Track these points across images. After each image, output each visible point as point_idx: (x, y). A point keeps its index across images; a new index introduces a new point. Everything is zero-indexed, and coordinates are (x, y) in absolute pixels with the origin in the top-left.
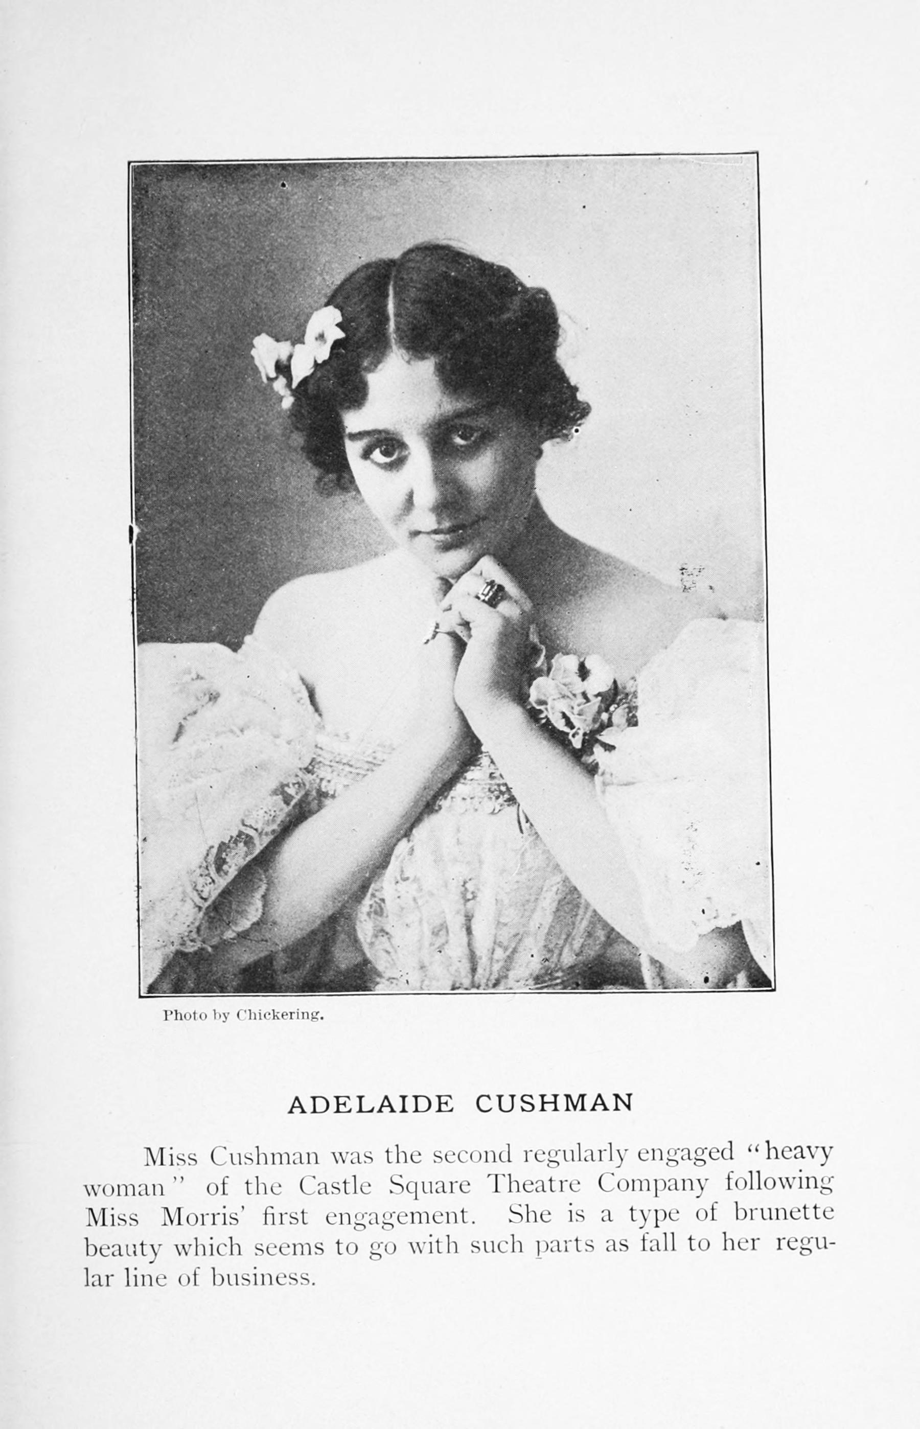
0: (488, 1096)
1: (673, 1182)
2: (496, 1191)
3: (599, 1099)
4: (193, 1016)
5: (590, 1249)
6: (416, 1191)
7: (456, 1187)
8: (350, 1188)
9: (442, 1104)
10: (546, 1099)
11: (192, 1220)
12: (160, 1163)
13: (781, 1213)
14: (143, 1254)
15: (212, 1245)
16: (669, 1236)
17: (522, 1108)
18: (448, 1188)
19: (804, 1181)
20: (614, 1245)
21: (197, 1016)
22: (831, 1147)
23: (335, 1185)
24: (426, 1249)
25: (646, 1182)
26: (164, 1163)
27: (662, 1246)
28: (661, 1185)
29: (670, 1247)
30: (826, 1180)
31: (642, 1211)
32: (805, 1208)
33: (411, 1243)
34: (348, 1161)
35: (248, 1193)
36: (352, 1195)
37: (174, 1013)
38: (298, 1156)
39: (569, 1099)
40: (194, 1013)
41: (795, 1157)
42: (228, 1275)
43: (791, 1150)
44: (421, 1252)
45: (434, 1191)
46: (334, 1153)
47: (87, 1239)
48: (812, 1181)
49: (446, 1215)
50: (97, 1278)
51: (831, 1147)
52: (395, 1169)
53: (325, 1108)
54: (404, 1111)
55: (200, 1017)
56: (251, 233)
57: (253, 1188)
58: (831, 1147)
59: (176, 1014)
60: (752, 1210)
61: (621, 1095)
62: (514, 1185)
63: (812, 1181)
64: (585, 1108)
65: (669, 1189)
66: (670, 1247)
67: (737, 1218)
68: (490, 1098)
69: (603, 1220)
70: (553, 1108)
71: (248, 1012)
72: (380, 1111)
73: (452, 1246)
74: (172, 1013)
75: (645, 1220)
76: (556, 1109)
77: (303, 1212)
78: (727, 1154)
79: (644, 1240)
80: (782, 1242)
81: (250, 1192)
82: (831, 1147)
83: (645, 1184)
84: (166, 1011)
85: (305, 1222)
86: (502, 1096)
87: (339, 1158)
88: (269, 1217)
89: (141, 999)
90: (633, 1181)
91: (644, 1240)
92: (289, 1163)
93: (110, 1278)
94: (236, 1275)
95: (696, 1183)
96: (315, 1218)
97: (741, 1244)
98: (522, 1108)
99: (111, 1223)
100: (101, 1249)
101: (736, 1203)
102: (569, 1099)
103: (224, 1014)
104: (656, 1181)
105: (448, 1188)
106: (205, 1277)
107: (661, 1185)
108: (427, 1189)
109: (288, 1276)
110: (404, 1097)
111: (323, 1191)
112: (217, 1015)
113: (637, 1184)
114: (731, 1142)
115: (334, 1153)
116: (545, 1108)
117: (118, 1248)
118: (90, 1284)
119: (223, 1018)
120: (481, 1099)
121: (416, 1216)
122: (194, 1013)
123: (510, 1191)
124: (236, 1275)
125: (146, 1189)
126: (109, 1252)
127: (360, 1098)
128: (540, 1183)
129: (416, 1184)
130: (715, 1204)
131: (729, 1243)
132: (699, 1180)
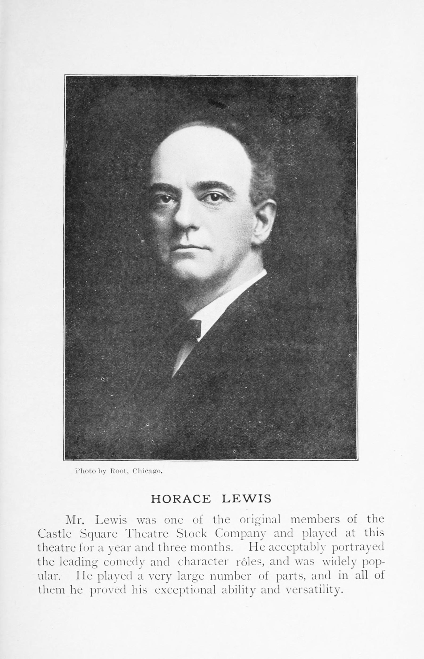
0: (199, 495)
1: (250, 533)
2: (130, 537)
4: (124, 471)
7: (111, 535)
8: (62, 534)
11: (86, 548)
12: (73, 523)
16: (365, 572)
21: (91, 471)
23: (55, 533)
26: (75, 523)
27: (361, 577)
28: (244, 534)
29: (365, 577)
34: (144, 523)
36: (369, 537)
37: (81, 470)
38: (103, 534)
40: (90, 470)
45: (100, 536)
46: (138, 519)
49: (161, 576)
55: (93, 471)
56: (277, 269)
57: (368, 534)
59: (82, 470)
62: (138, 534)
66: (365, 577)
68: (199, 497)
70: (158, 501)
71: (138, 470)
74: (79, 470)
76: (159, 502)
79: (80, 546)
83: (237, 534)
84: (111, 469)
85: (354, 535)
91: (80, 546)
92: (270, 522)
95: (260, 534)
103: (103, 470)
105: (197, 563)
107: (244, 534)
108: (98, 535)
111: (49, 536)
112: (100, 471)
113: (119, 562)
116: (154, 501)
119: (103, 472)
120: (195, 497)
121: (59, 590)
122: (90, 470)
123: (136, 537)
128: (150, 533)
129: (92, 533)
131: (73, 590)
132: (262, 532)
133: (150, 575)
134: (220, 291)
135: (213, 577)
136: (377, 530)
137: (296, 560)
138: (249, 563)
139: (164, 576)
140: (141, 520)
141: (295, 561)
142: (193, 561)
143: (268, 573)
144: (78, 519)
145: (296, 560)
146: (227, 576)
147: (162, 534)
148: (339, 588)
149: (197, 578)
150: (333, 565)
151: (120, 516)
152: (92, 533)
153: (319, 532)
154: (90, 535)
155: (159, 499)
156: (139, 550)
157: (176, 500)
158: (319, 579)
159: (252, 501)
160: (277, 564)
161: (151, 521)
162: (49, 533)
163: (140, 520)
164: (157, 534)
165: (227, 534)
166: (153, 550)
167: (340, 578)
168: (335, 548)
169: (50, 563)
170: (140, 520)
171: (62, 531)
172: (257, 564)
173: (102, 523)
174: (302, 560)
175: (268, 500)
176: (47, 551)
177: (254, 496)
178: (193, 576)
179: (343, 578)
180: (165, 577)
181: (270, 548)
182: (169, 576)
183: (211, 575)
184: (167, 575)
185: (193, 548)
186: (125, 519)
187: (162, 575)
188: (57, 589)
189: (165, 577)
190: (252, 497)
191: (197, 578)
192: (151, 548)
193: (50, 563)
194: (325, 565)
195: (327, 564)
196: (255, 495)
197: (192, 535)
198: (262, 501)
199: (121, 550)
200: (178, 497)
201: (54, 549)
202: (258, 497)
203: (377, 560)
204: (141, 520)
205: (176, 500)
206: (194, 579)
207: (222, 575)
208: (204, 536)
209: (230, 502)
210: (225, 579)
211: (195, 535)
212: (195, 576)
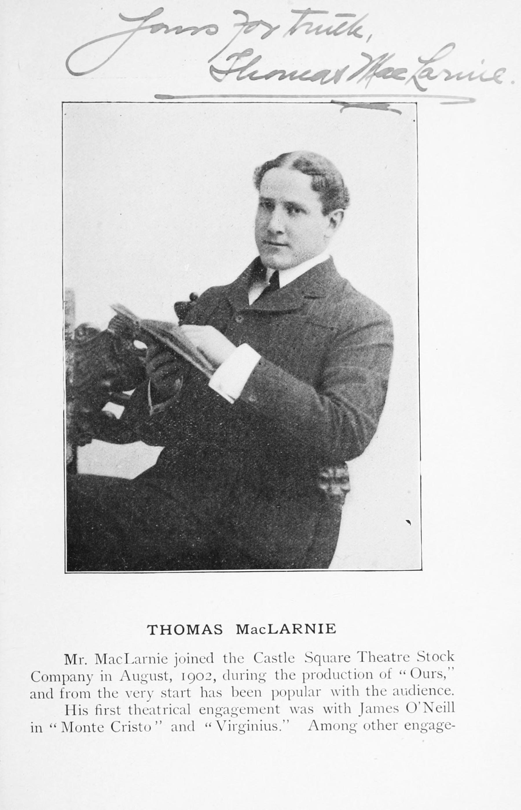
1: (73, 676)
3: (285, 627)
6: (320, 661)
10: (164, 628)
13: (41, 695)
14: (340, 712)
17: (215, 632)
24: (333, 711)
25: (58, 676)
26: (76, 663)
28: (66, 678)
30: (262, 675)
33: (291, 708)
41: (385, 661)
43: (382, 657)
44: (297, 712)
45: (330, 661)
48: (254, 676)
49: (429, 690)
52: (228, 666)
57: (279, 676)
60: (312, 674)
61: (191, 626)
63: (254, 676)
64: (199, 632)
65: (71, 680)
66: (451, 710)
67: (233, 696)
68: (157, 627)
69: (394, 694)
72: (281, 633)
73: (348, 709)
75: (150, 697)
76: (170, 633)
77: (118, 708)
78: (210, 660)
79: (62, 692)
83: (57, 677)
88: (99, 711)
90: (367, 673)
91: (62, 692)
93: (396, 725)
94: (270, 725)
97: (438, 709)
98: (215, 632)
99: (372, 694)
100: (241, 692)
101: (233, 687)
104: (63, 676)
107: (66, 678)
108: (326, 659)
113: (53, 678)
117: (183, 710)
121: (251, 710)
126: (148, 712)
127: (270, 625)
130: (63, 689)
132: (88, 675)
134: (339, 183)
137: (291, 708)
139: (125, 727)
141: (323, 708)
146: (377, 709)
147: (401, 658)
149: (238, 712)
150: (171, 713)
151: (176, 654)
152: (320, 657)
153: (87, 676)
155: (169, 629)
156: (35, 697)
157: (296, 630)
158: (257, 730)
162: (267, 658)
164: (396, 658)
165: (45, 678)
166: (304, 674)
167: (32, 731)
168: (276, 693)
169: (260, 711)
171: (283, 655)
172: (393, 712)
173: (133, 663)
174: (299, 707)
175: (219, 632)
178: (239, 726)
181: (394, 691)
187: (394, 724)
188: (413, 724)
189: (146, 694)
192: (49, 695)
193: (260, 711)
194: (293, 712)
198: (248, 632)
200: (299, 626)
205: (296, 630)
208: (450, 659)
211: (440, 658)
212: (241, 726)
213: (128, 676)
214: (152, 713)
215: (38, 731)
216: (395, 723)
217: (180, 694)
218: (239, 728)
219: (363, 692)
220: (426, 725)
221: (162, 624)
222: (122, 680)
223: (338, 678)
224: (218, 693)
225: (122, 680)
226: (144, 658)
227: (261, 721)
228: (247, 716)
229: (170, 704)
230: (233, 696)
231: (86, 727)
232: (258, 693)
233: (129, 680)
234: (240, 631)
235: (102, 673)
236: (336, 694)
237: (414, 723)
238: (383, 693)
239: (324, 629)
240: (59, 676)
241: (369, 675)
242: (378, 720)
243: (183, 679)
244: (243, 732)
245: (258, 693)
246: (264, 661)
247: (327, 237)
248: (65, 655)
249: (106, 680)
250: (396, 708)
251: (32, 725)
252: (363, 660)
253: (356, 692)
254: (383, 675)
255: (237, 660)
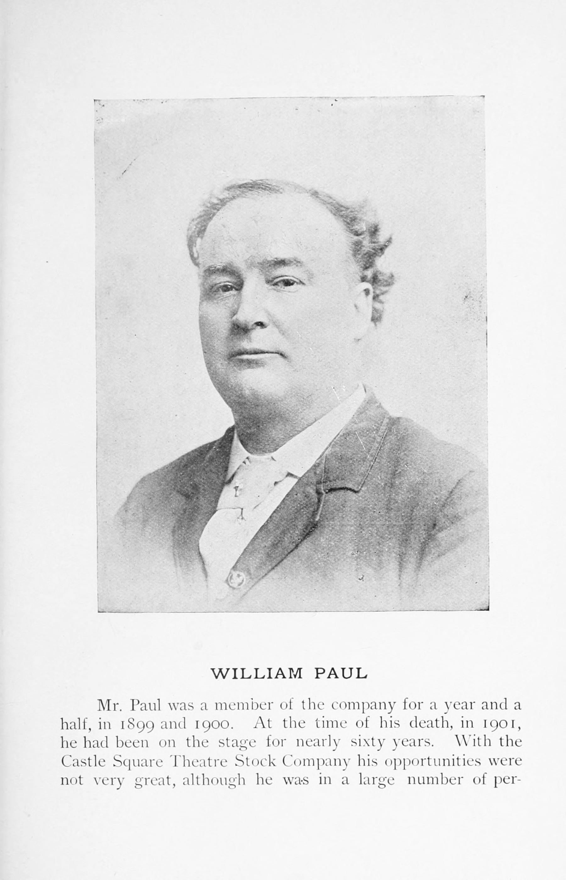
5: (478, 764)
7: (154, 763)
9: (297, 673)
12: (107, 709)
14: (458, 765)
15: (464, 759)
18: (148, 763)
19: (326, 723)
20: (78, 763)
22: (395, 703)
26: (110, 709)
31: (119, 779)
32: (373, 739)
34: (178, 709)
35: (285, 727)
39: (291, 671)
42: (221, 779)
44: (496, 764)
45: (140, 765)
46: (169, 704)
47: (359, 755)
49: (458, 779)
50: (367, 779)
51: (395, 703)
53: (349, 676)
54: (270, 677)
57: (287, 724)
58: (395, 703)
62: (187, 762)
79: (268, 740)
80: (512, 760)
81: (286, 726)
82: (395, 703)
86: (301, 668)
87: (173, 706)
89: (99, 613)
91: (268, 740)
93: (461, 779)
96: (214, 743)
102: (291, 671)
105: (148, 763)
106: (251, 779)
108: (136, 764)
109: (474, 760)
110: (343, 669)
111: (76, 764)
113: (307, 762)
114: (366, 677)
115: (169, 704)
118: (363, 783)
121: (241, 705)
124: (226, 779)
125: (432, 724)
127: (243, 669)
128: (430, 722)
133: (95, 778)
135: (412, 780)
136: (391, 719)
137: (490, 759)
138: (455, 762)
140: (174, 705)
142: (144, 761)
143: (485, 775)
144: (114, 704)
145: (490, 759)
148: (123, 778)
149: (386, 782)
154: (127, 763)
159: (224, 677)
160: (150, 765)
161: (187, 707)
162: (76, 761)
163: (172, 705)
164: (212, 763)
170: (172, 705)
176: (67, 747)
177: (226, 670)
178: (379, 779)
179: (325, 783)
180: (116, 782)
182: (121, 780)
183: (409, 778)
184: (119, 779)
185: (219, 706)
186: (192, 703)
189: (116, 782)
190: (224, 671)
191: (386, 782)
195: (494, 764)
196: (228, 669)
197: (255, 762)
199: (233, 746)
201: (312, 743)
202: (231, 672)
203: (395, 759)
204: (174, 705)
206: (381, 783)
207: (423, 777)
209: (265, 677)
210: (325, 783)
212: (382, 780)
213: (262, 723)
214: (430, 726)
215: (411, 782)
216: (460, 777)
217: (417, 743)
218: (379, 781)
219: (496, 742)
220: (384, 779)
221: (343, 667)
222: (256, 727)
223: (416, 727)
224: (352, 742)
225: (256, 727)
226: (471, 703)
227: (320, 773)
228: (442, 769)
229: (453, 755)
230: (118, 746)
231: (411, 779)
232: (145, 743)
233: (264, 727)
234: (293, 676)
235: (100, 720)
236: (174, 709)
237: (429, 777)
238: (302, 725)
239: (239, 674)
240: (337, 722)
241: (172, 742)
242: (203, 774)
243: (485, 727)
244: (140, 786)
245: (145, 743)
246: (72, 765)
247: (366, 201)
248: (98, 700)
249: (105, 728)
250: (478, 760)
251: (320, 775)
252: (420, 708)
253: (488, 742)
254: (360, 724)
255: (317, 706)
